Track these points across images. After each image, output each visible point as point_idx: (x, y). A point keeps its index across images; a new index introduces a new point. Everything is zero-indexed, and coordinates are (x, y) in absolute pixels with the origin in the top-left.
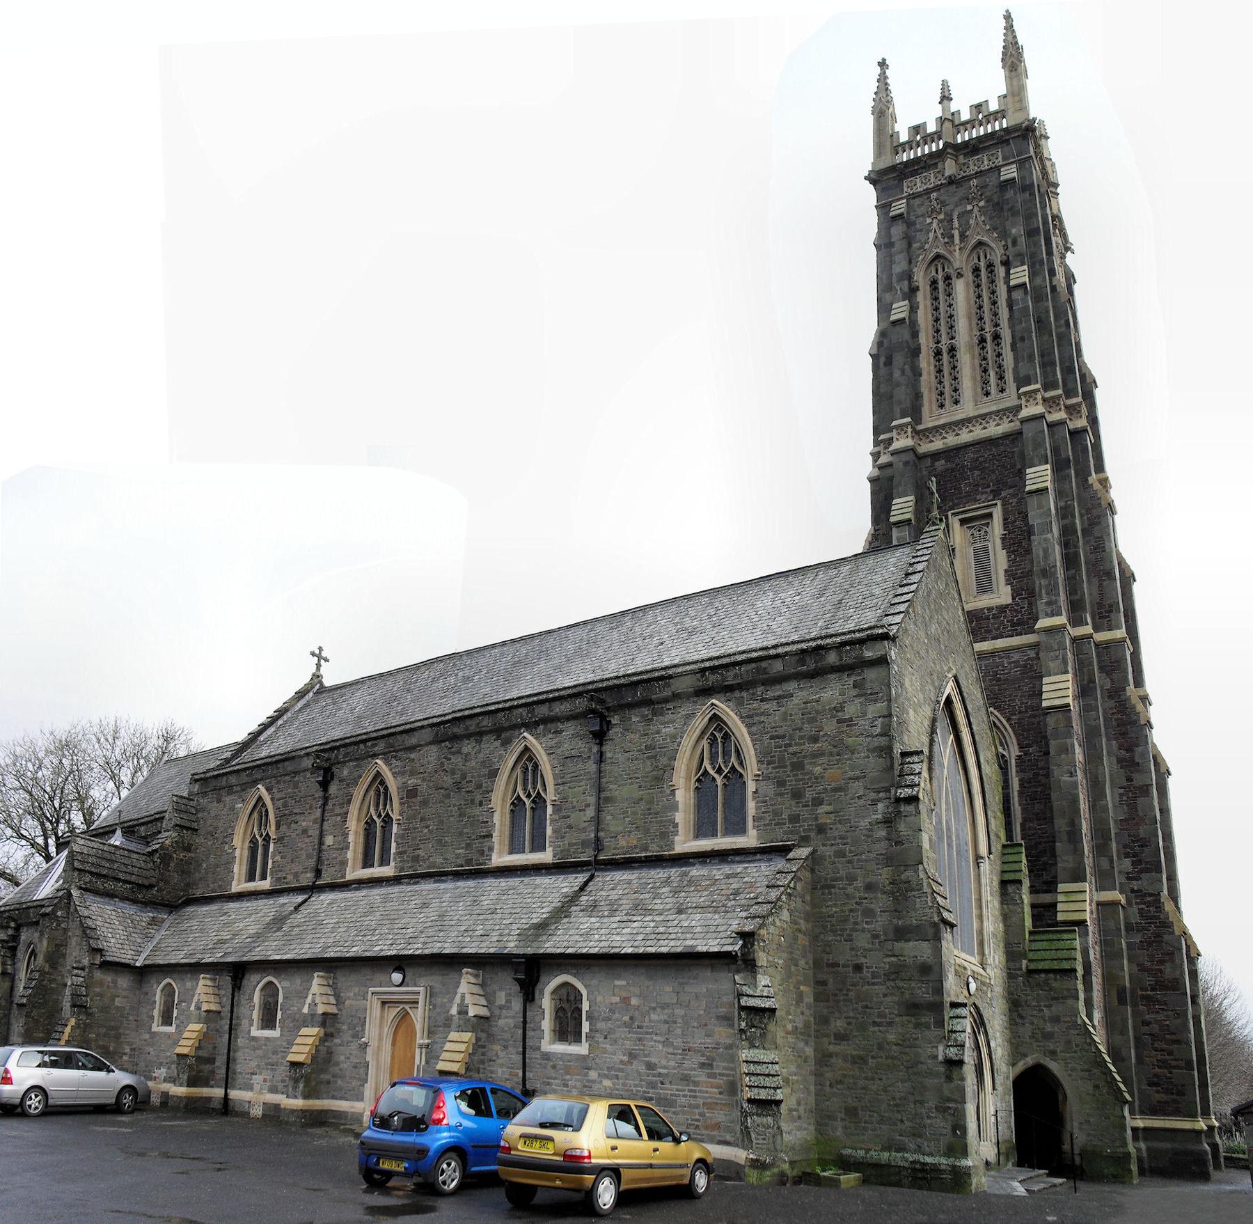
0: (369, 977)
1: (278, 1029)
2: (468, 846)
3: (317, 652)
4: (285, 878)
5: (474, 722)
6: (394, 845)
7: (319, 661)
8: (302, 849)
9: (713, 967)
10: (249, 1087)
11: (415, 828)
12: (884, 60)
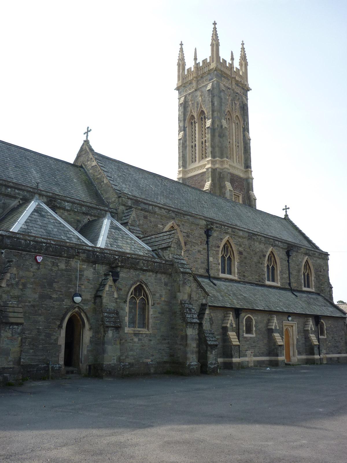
0: (281, 318)
1: (255, 334)
2: (259, 276)
5: (260, 237)
8: (199, 259)
10: (245, 356)
11: (243, 266)
12: (215, 22)
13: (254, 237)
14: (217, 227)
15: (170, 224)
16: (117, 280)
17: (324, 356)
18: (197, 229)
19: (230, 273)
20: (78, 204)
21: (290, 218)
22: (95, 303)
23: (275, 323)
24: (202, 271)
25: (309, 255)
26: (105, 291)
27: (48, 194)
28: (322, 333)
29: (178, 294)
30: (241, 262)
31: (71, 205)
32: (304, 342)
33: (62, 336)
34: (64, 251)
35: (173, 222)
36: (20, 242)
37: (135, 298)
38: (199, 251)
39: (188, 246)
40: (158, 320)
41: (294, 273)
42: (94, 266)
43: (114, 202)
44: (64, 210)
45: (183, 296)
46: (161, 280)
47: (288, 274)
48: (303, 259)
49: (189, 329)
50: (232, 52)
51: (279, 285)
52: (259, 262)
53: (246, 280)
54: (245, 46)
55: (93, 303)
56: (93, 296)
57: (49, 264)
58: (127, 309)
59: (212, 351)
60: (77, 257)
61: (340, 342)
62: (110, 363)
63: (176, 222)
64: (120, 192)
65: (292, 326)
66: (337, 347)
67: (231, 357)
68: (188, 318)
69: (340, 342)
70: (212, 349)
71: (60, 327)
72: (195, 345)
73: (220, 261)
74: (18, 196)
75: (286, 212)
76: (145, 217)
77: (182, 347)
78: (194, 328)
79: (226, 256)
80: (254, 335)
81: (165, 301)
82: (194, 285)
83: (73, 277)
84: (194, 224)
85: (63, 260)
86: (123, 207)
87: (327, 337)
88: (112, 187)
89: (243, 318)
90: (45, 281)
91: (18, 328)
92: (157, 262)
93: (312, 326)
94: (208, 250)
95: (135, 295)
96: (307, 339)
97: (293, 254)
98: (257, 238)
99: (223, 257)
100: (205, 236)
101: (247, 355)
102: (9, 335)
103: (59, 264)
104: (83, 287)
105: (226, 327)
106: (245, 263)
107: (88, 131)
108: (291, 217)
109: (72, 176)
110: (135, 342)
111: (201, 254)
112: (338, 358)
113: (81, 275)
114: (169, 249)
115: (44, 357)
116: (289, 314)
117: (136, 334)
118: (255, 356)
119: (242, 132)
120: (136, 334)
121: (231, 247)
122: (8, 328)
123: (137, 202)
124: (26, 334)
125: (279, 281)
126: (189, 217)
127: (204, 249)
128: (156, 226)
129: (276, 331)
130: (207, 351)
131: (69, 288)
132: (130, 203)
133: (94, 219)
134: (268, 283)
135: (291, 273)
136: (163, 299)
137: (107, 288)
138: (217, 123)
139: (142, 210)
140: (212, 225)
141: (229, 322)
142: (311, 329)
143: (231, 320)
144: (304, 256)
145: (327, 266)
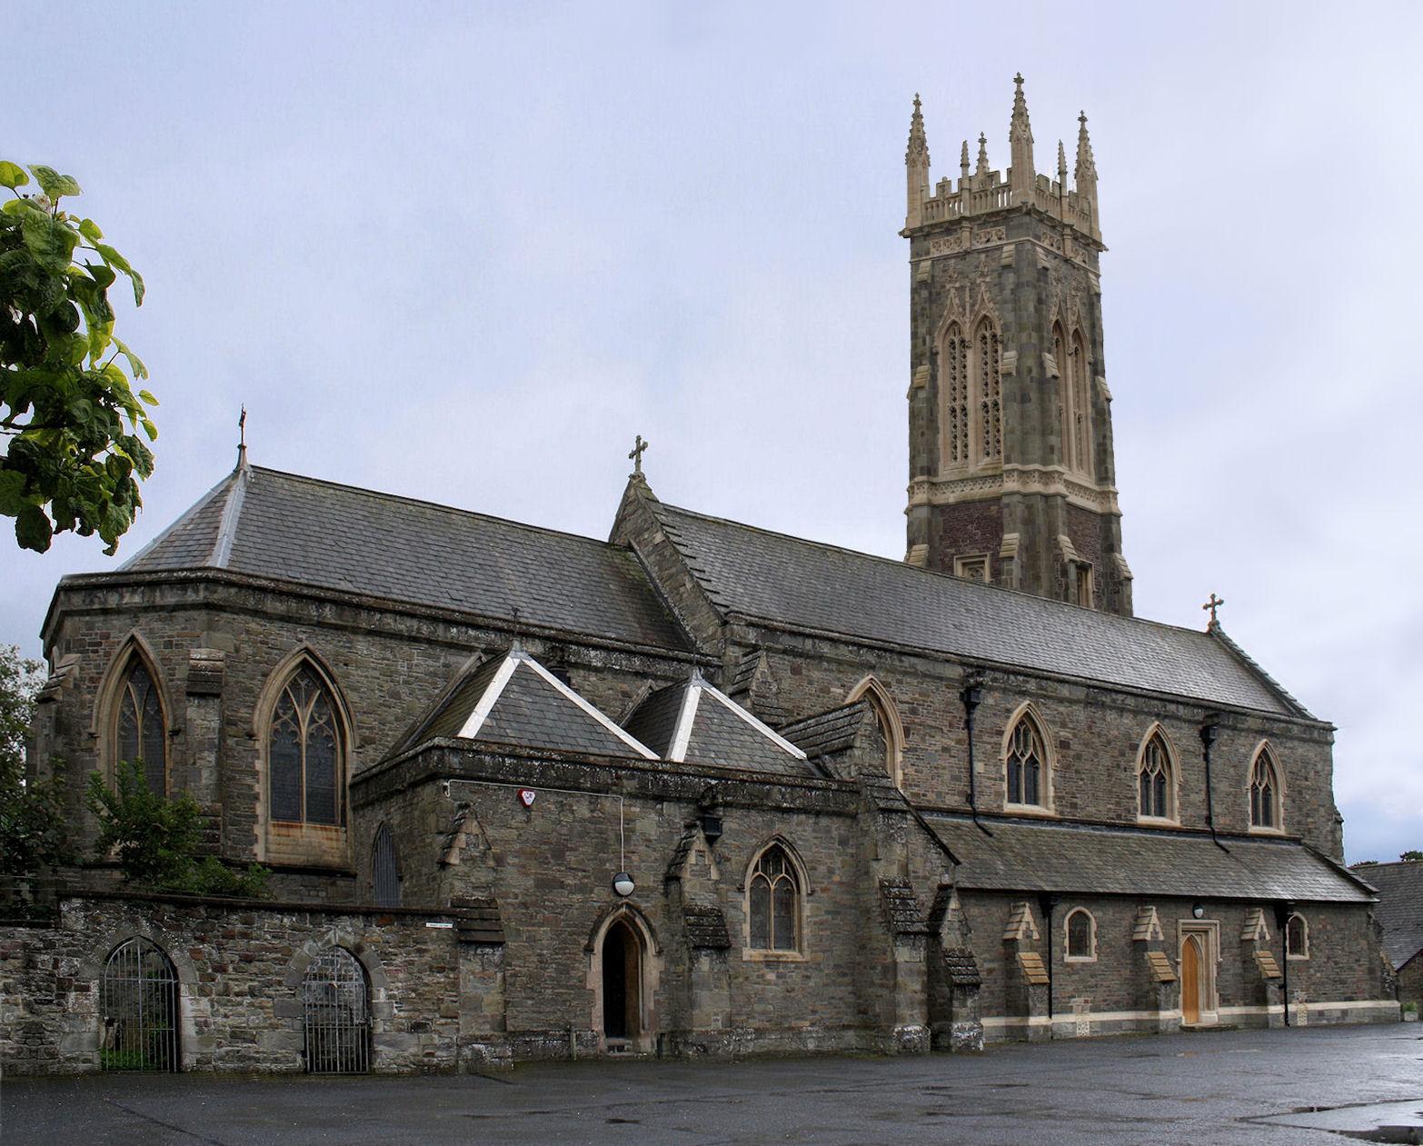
2: (1118, 804)
3: (1216, 600)
4: (924, 795)
5: (1120, 697)
6: (1250, 812)
7: (1210, 606)
8: (944, 768)
9: (1358, 909)
10: (1069, 1010)
13: (1104, 699)
14: (994, 680)
15: (864, 681)
16: (717, 837)
17: (1302, 1007)
18: (937, 690)
19: (1034, 800)
20: (621, 651)
21: (1224, 630)
22: (666, 894)
23: (1152, 924)
24: (954, 801)
25: (1272, 735)
26: (688, 866)
27: (547, 632)
28: (1297, 947)
29: (875, 865)
30: (1064, 769)
31: (604, 654)
32: (1240, 971)
33: (593, 969)
34: (584, 776)
35: (870, 676)
36: (480, 760)
37: (765, 879)
38: (945, 749)
39: (914, 738)
40: (826, 929)
41: (1222, 786)
42: (659, 806)
43: (712, 637)
44: (589, 670)
45: (887, 870)
46: (829, 832)
47: (1203, 793)
48: (1253, 746)
49: (901, 949)
51: (1176, 823)
52: (1118, 766)
53: (1080, 815)
55: (662, 894)
56: (661, 877)
57: (552, 807)
58: (746, 906)
59: (965, 1000)
60: (614, 788)
61: (1351, 969)
62: (709, 1029)
63: (877, 676)
64: (727, 610)
65: (1206, 932)
66: (1343, 982)
67: (1027, 1013)
68: (897, 921)
69: (1351, 969)
70: (965, 994)
71: (589, 950)
72: (918, 987)
73: (1005, 772)
74: (476, 645)
75: (1214, 613)
76: (796, 671)
77: (885, 992)
78: (914, 944)
79: (1022, 755)
80: (1092, 958)
81: (841, 883)
82: (918, 840)
83: (611, 835)
84: (929, 676)
85: (582, 796)
86: (736, 649)
87: (1311, 955)
88: (706, 598)
89: (1064, 917)
90: (547, 847)
91: (493, 954)
92: (818, 789)
93: (1265, 930)
94: (970, 744)
95: (765, 871)
96: (1248, 962)
97: (1221, 738)
98: (1114, 701)
99: (1014, 759)
100: (962, 706)
101: (1072, 1007)
102: (478, 968)
103: (575, 808)
104: (635, 858)
105: (1014, 940)
106: (1077, 772)
107: (641, 448)
108: (1228, 629)
109: (539, 612)
110: (769, 983)
111: (951, 756)
112: (1345, 1012)
113: (630, 832)
114: (849, 752)
115: (559, 1014)
116: (1196, 901)
117: (768, 964)
118: (1095, 1009)
120: (768, 964)
121: (1037, 731)
122: (472, 952)
123: (767, 629)
124: (515, 966)
125: (1176, 813)
126: (913, 660)
127: (959, 742)
128: (825, 690)
129: (1156, 944)
130: (951, 999)
131: (603, 862)
132: (752, 636)
133: (665, 685)
134: (1142, 819)
135: (1214, 789)
136: (836, 878)
137: (692, 858)
139: (785, 652)
140: (979, 674)
141: (1023, 927)
142: (1262, 937)
143: (1028, 923)
144: (1254, 738)
145: (1328, 761)
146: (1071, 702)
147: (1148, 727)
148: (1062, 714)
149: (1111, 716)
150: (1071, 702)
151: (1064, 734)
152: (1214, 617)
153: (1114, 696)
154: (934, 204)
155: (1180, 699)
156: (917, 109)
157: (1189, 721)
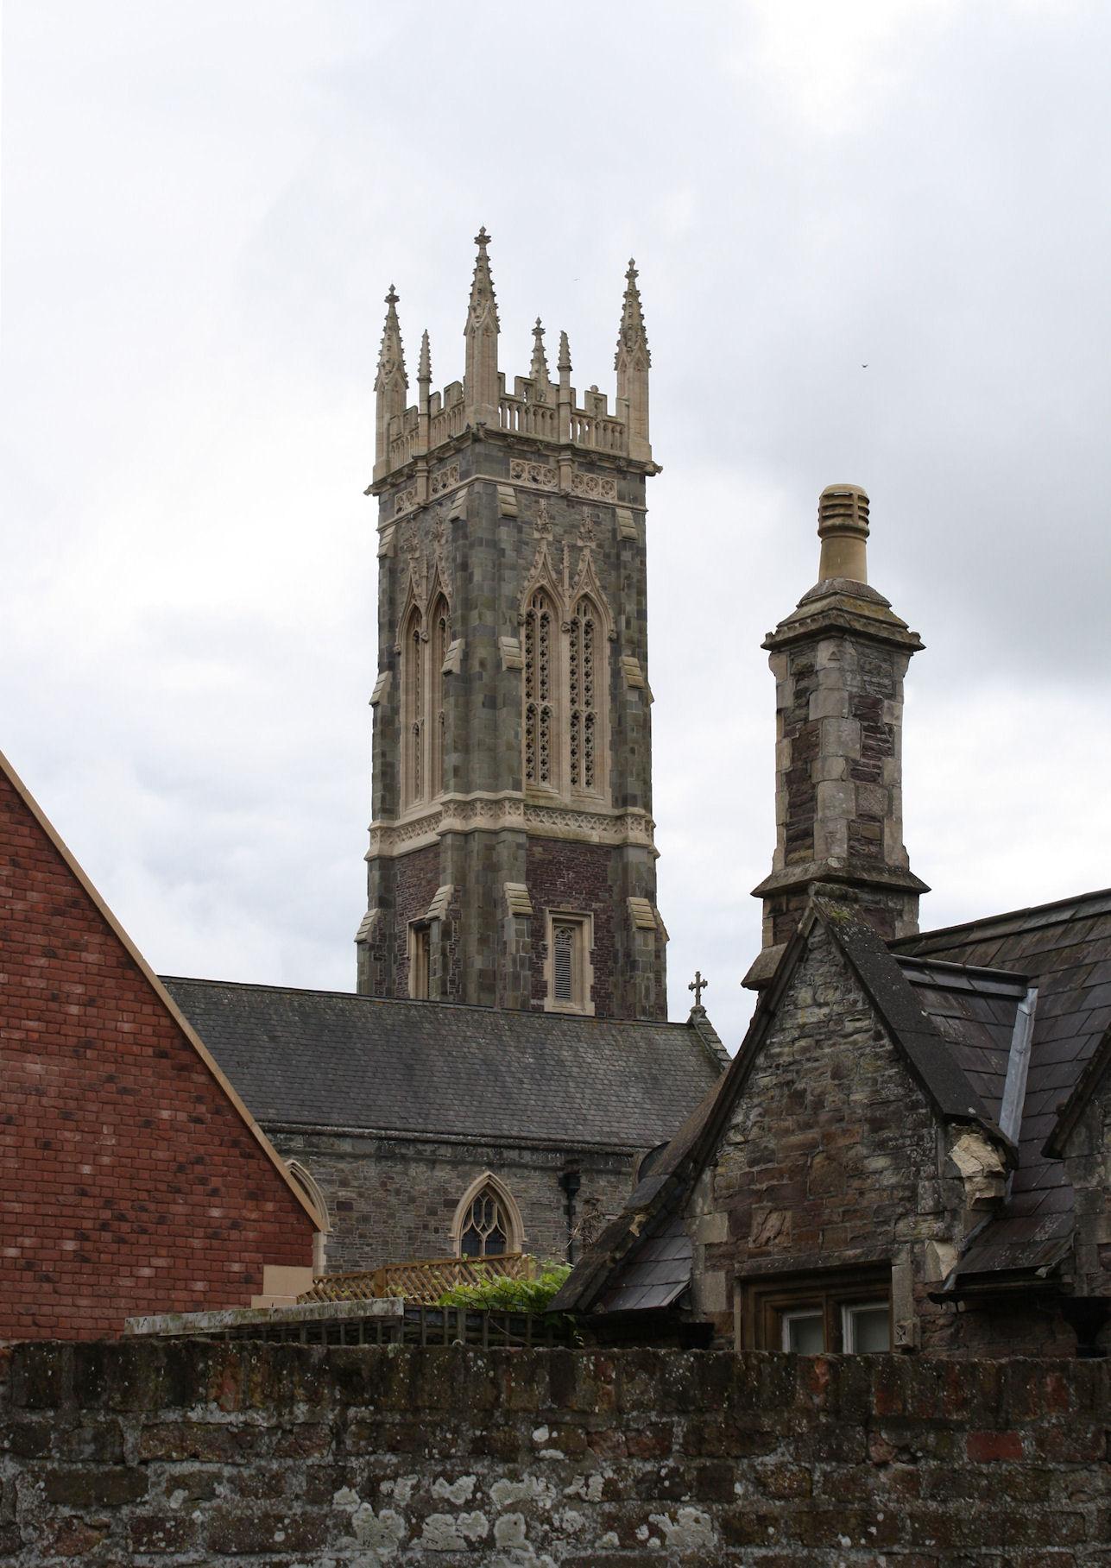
5: (429, 1148)
50: (564, 335)
52: (426, 1227)
54: (639, 283)
75: (698, 996)
98: (419, 1152)
119: (606, 662)
138: (481, 652)
146: (356, 1157)
147: (475, 1178)
148: (343, 1171)
149: (416, 1170)
150: (356, 1157)
151: (343, 1194)
152: (698, 1001)
153: (420, 1147)
154: (610, 426)
155: (523, 1143)
156: (632, 285)
157: (542, 1169)
